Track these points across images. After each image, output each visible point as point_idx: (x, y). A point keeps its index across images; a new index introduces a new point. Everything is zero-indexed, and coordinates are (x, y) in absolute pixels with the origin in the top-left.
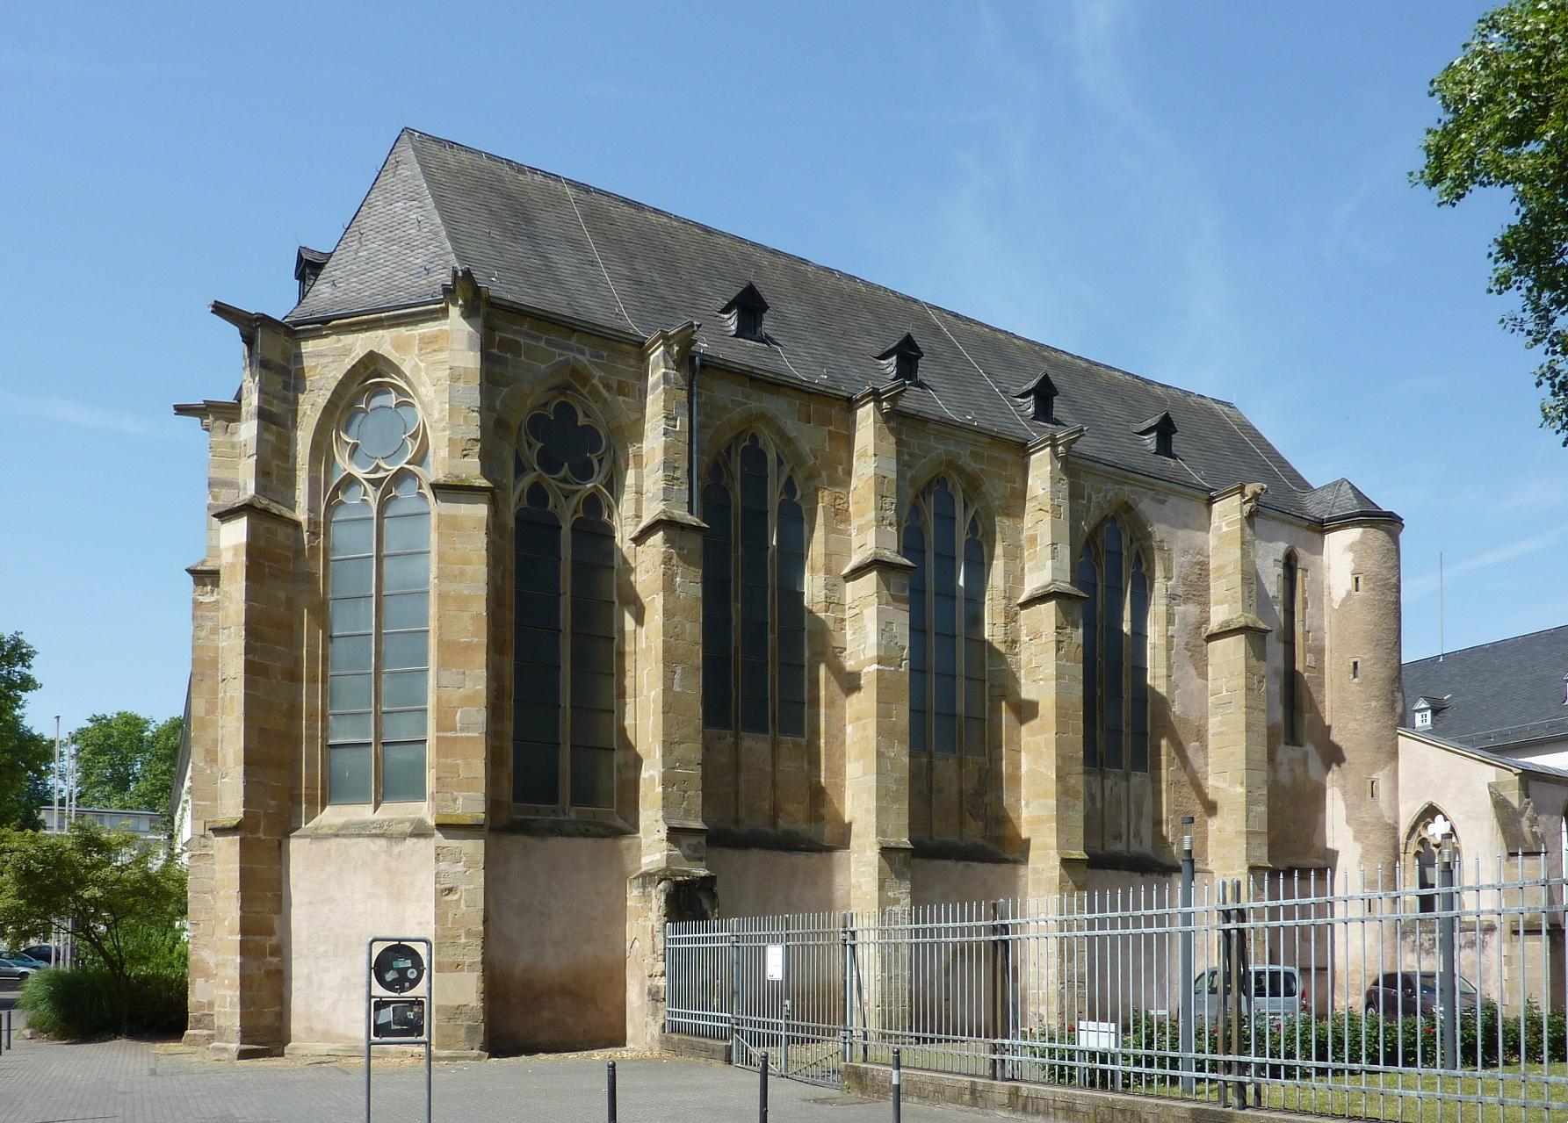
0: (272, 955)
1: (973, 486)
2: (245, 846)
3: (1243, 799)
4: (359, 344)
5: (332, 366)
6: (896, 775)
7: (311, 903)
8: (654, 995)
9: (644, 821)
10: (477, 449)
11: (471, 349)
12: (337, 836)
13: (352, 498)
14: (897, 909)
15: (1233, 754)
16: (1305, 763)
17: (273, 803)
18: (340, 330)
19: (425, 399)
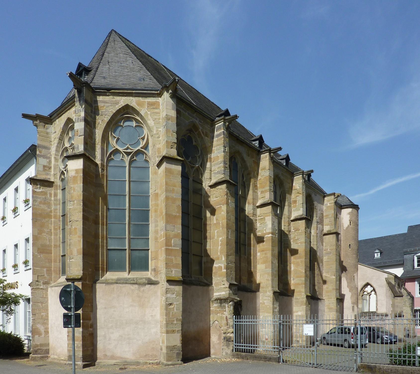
0: (91, 328)
3: (335, 280)
4: (123, 101)
5: (111, 107)
7: (105, 308)
9: (215, 280)
10: (175, 146)
11: (173, 109)
12: (117, 283)
13: (117, 158)
15: (331, 267)
17: (90, 270)
19: (150, 125)
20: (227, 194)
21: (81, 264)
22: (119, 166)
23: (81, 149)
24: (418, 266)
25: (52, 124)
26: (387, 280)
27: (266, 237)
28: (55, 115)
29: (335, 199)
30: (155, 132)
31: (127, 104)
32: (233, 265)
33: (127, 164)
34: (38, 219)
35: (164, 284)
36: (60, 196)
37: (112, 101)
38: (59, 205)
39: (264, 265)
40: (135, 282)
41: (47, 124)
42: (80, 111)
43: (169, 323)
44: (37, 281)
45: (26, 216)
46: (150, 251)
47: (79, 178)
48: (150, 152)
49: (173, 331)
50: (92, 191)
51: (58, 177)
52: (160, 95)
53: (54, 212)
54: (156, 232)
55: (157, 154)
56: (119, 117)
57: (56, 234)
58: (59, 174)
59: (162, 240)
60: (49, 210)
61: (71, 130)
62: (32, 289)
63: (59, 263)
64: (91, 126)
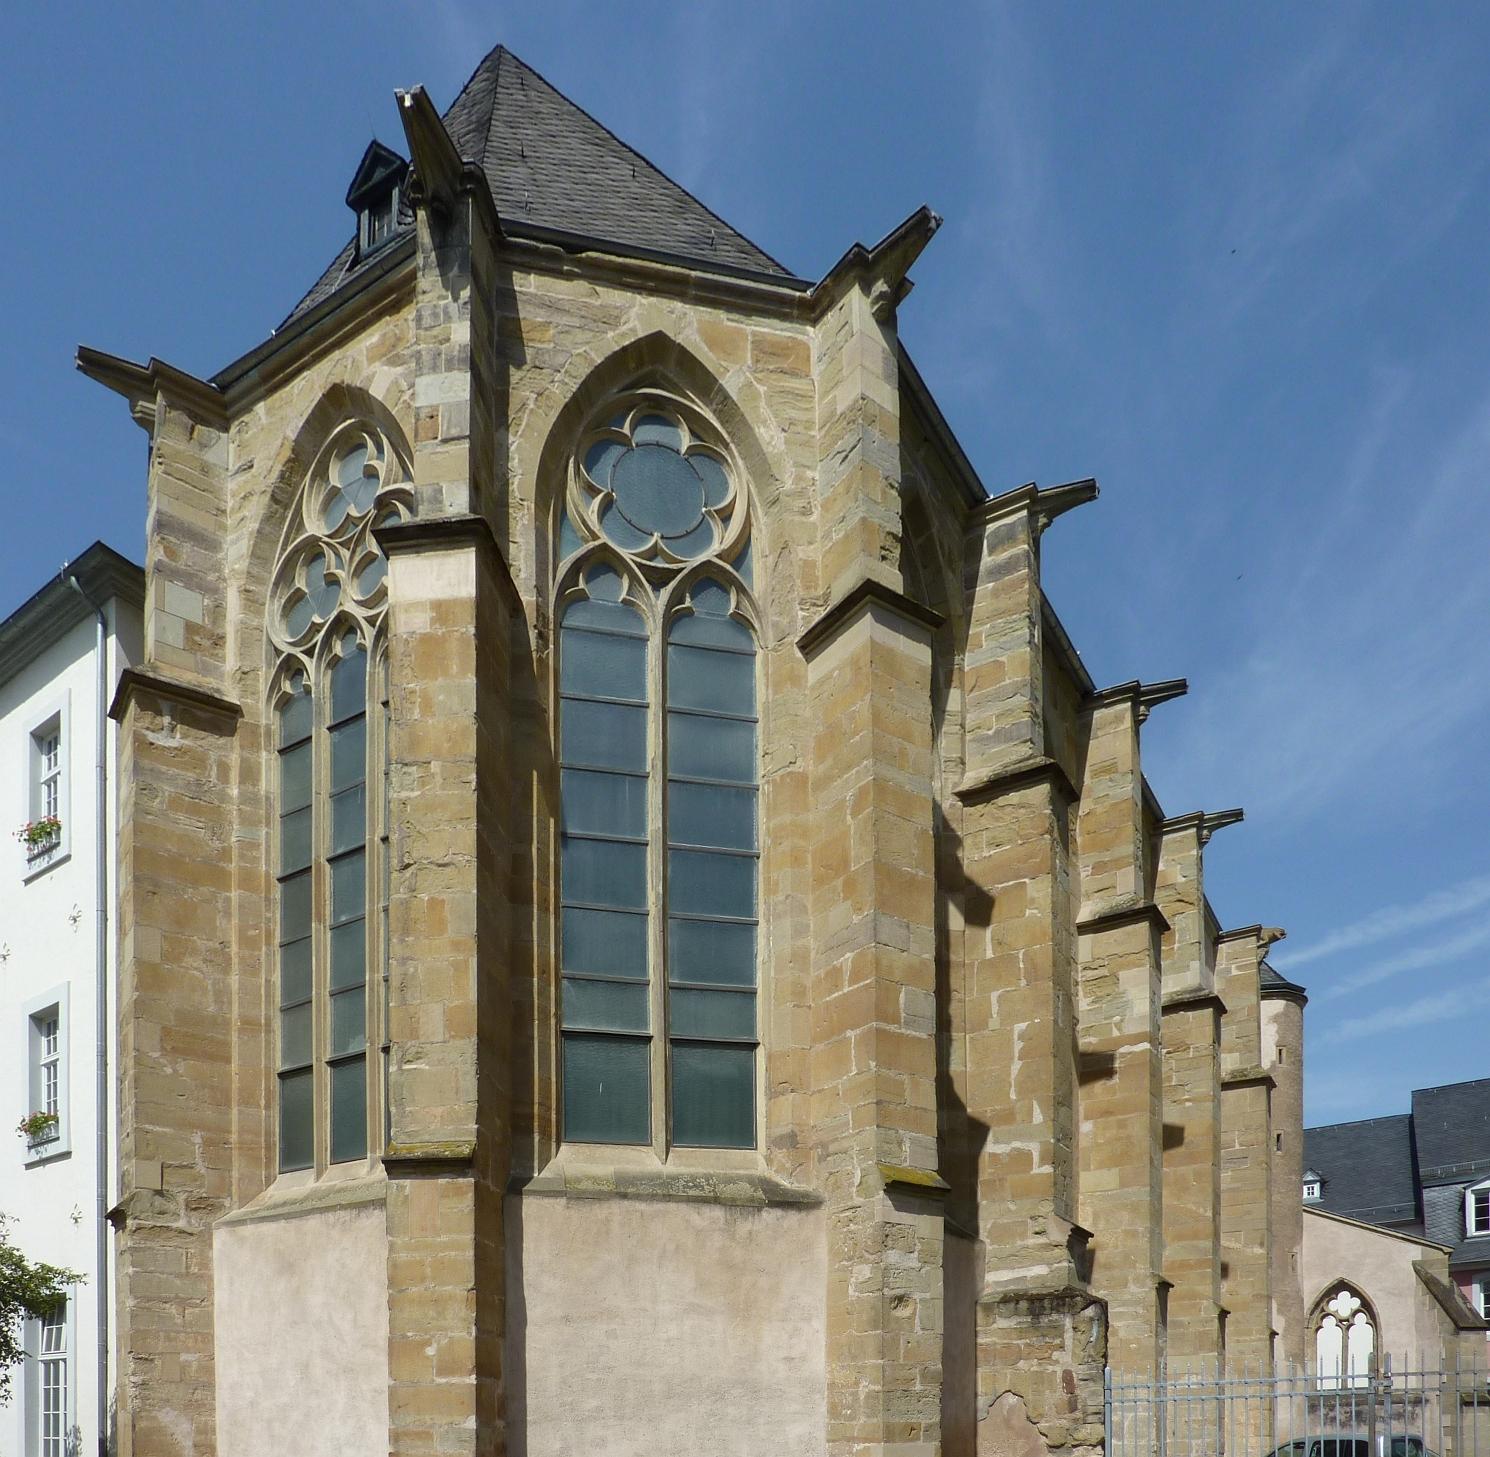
4: (640, 315)
5: (580, 336)
7: (567, 1319)
12: (624, 1196)
15: (1249, 1213)
18: (599, 274)
22: (612, 634)
23: (456, 503)
24: (1480, 1226)
25: (226, 430)
26: (1418, 1269)
27: (1123, 1055)
28: (254, 375)
29: (1262, 951)
30: (788, 484)
31: (660, 332)
37: (586, 305)
38: (268, 824)
39: (1115, 1171)
40: (702, 1195)
41: (207, 423)
42: (448, 318)
44: (159, 1193)
46: (760, 1052)
47: (453, 646)
48: (759, 575)
51: (263, 687)
52: (811, 311)
53: (242, 856)
55: (800, 591)
56: (613, 393)
57: (250, 968)
61: (342, 457)
63: (268, 1107)
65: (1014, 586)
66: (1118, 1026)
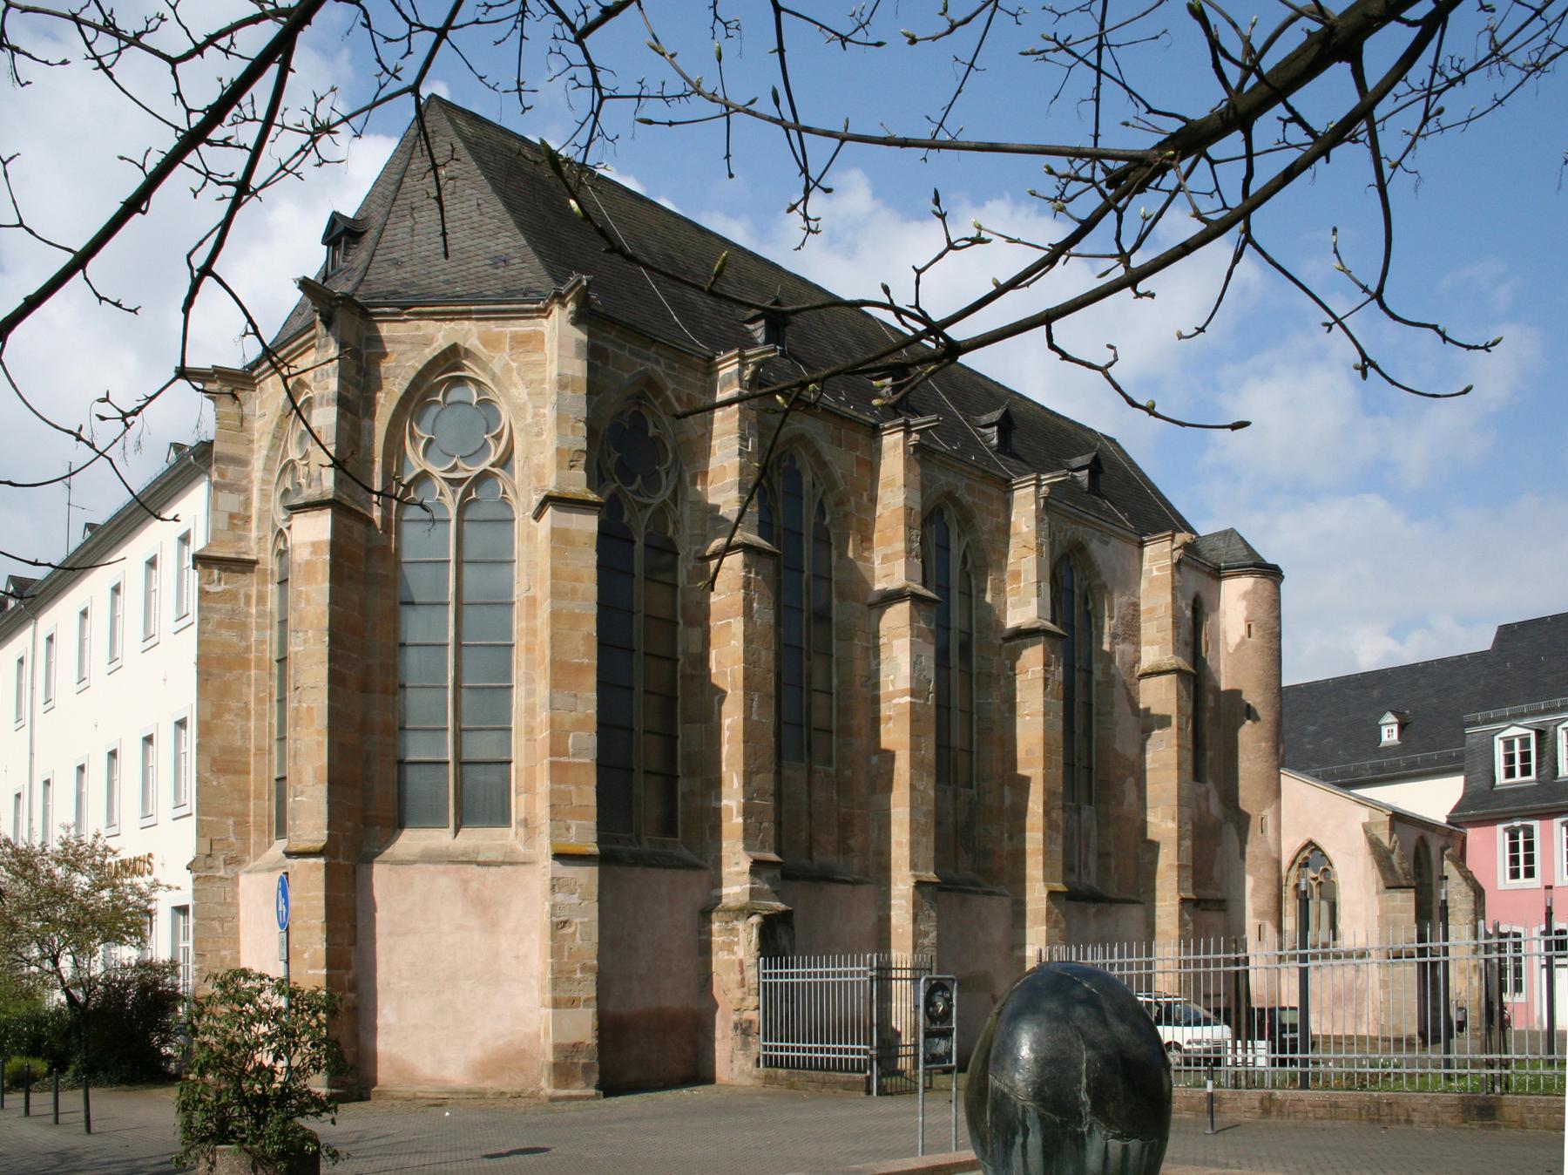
1: (966, 520)
2: (330, 871)
4: (441, 334)
5: (410, 355)
6: (925, 808)
8: (744, 1029)
10: (583, 461)
14: (926, 941)
16: (1207, 799)
17: (349, 824)
20: (747, 585)
21: (324, 808)
26: (1367, 828)
32: (769, 803)
33: (453, 513)
34: (216, 669)
35: (546, 865)
36: (272, 603)
43: (559, 977)
45: (181, 652)
49: (573, 1002)
50: (356, 598)
51: (269, 545)
52: (544, 312)
54: (530, 711)
55: (534, 483)
57: (261, 716)
58: (270, 538)
59: (543, 735)
60: (244, 644)
62: (196, 880)
64: (356, 414)
65: (731, 416)
66: (893, 682)
